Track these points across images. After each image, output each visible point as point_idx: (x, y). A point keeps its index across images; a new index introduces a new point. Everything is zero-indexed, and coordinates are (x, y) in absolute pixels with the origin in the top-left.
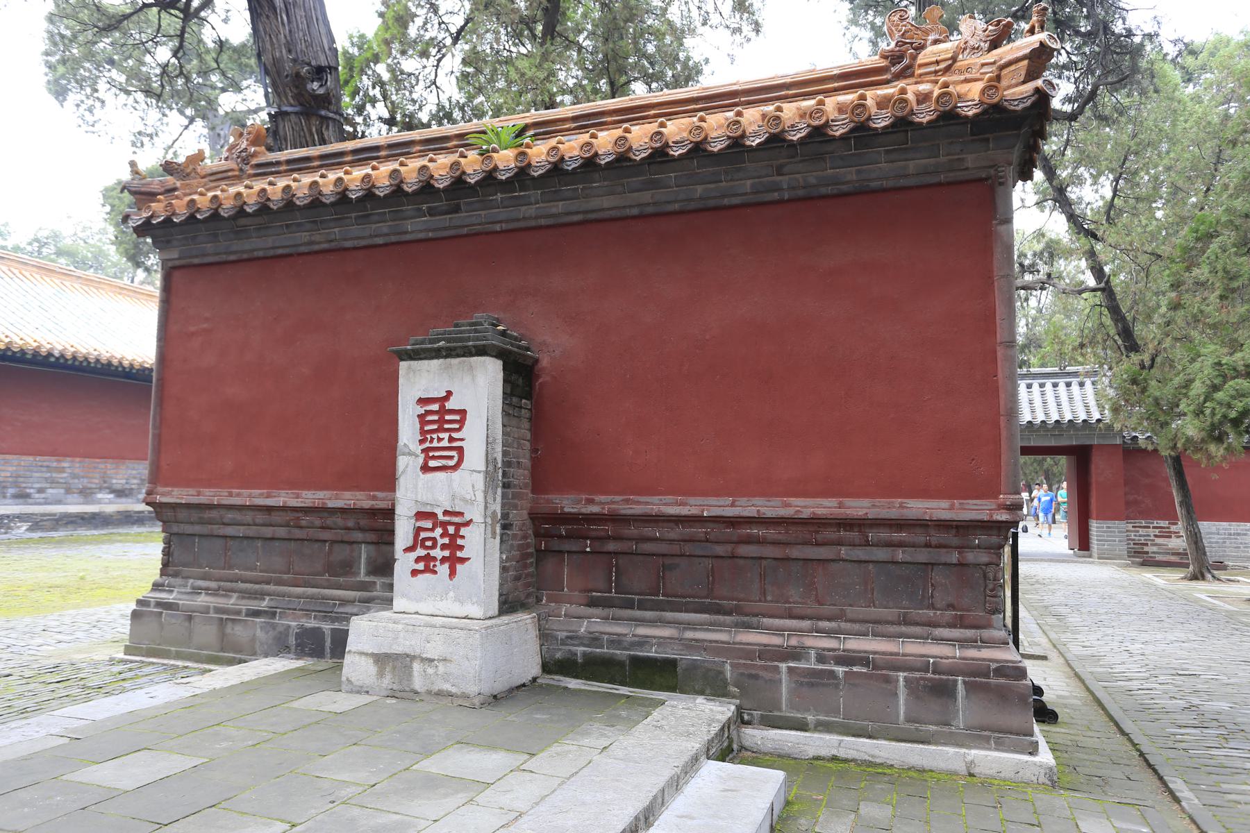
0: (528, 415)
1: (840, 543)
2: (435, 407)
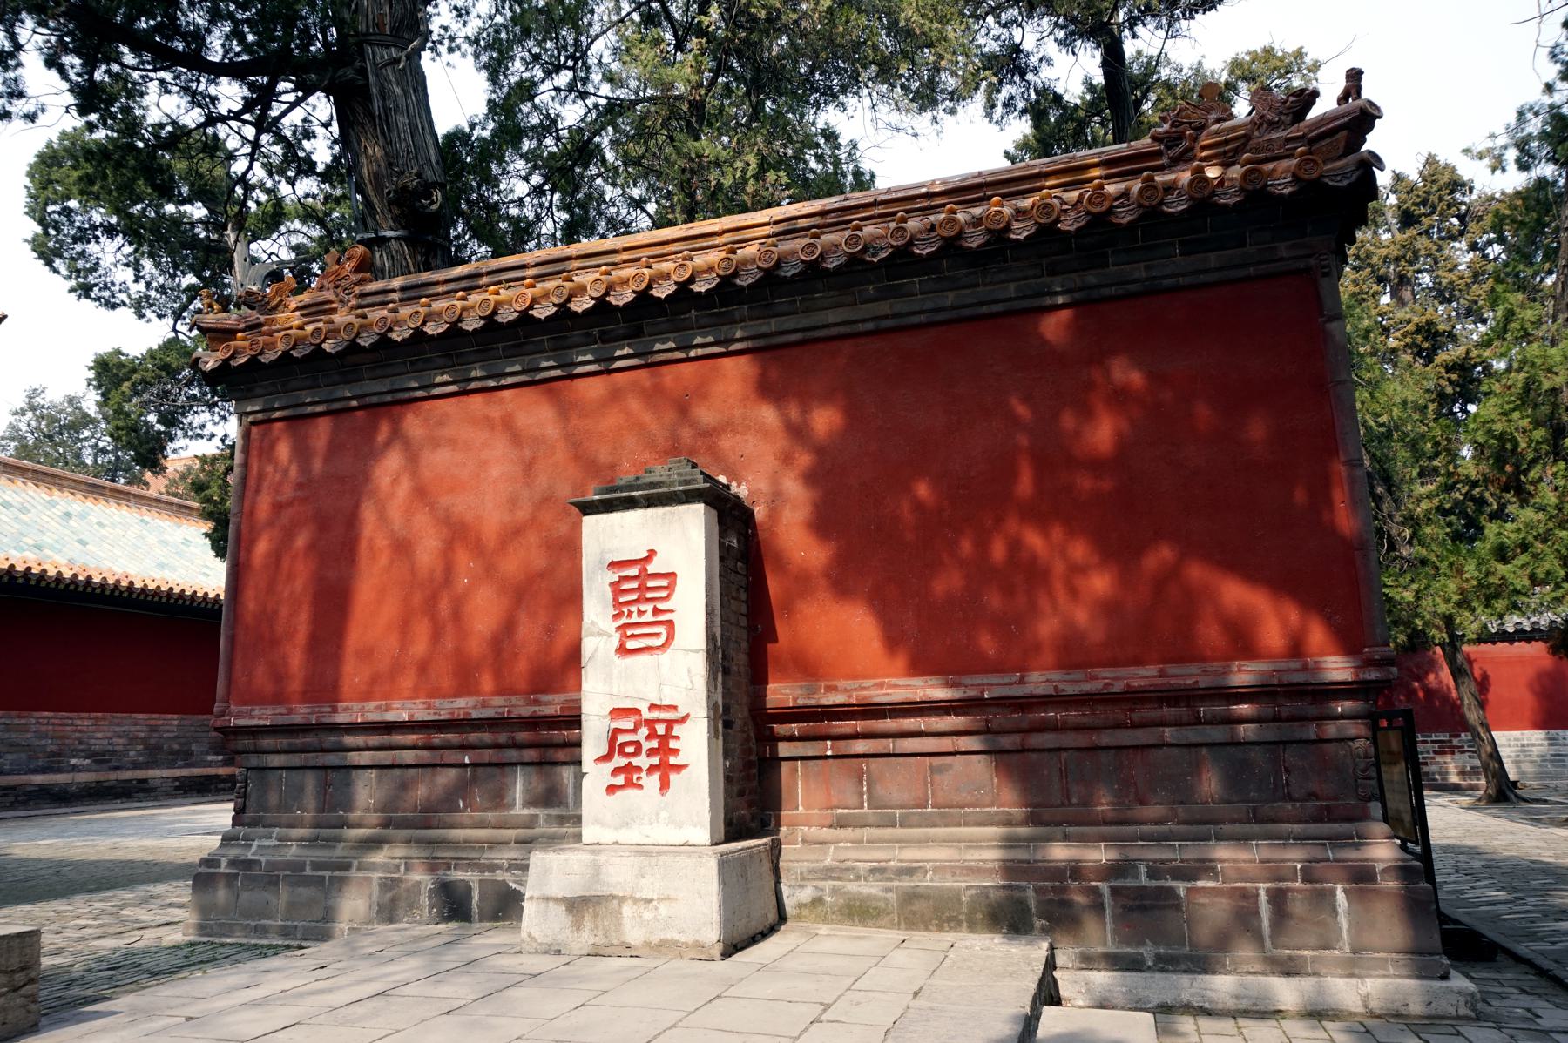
0: (744, 583)
1: (1164, 723)
2: (634, 572)
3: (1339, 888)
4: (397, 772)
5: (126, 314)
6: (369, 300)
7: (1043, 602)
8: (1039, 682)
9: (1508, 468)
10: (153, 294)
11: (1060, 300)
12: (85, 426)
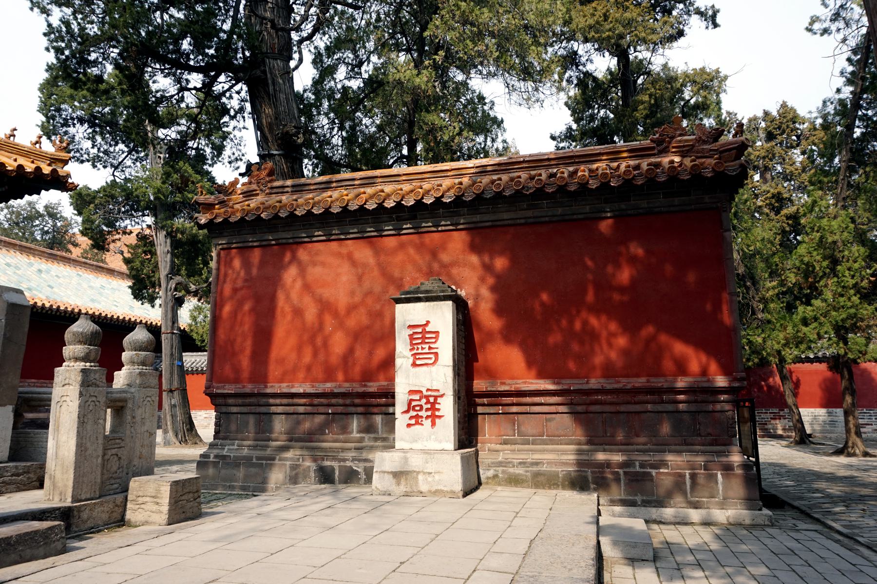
2: (420, 330)
3: (719, 473)
4: (295, 416)
5: (88, 165)
6: (275, 190)
7: (597, 349)
8: (594, 383)
9: (810, 280)
10: (101, 155)
11: (609, 215)
12: (37, 219)
